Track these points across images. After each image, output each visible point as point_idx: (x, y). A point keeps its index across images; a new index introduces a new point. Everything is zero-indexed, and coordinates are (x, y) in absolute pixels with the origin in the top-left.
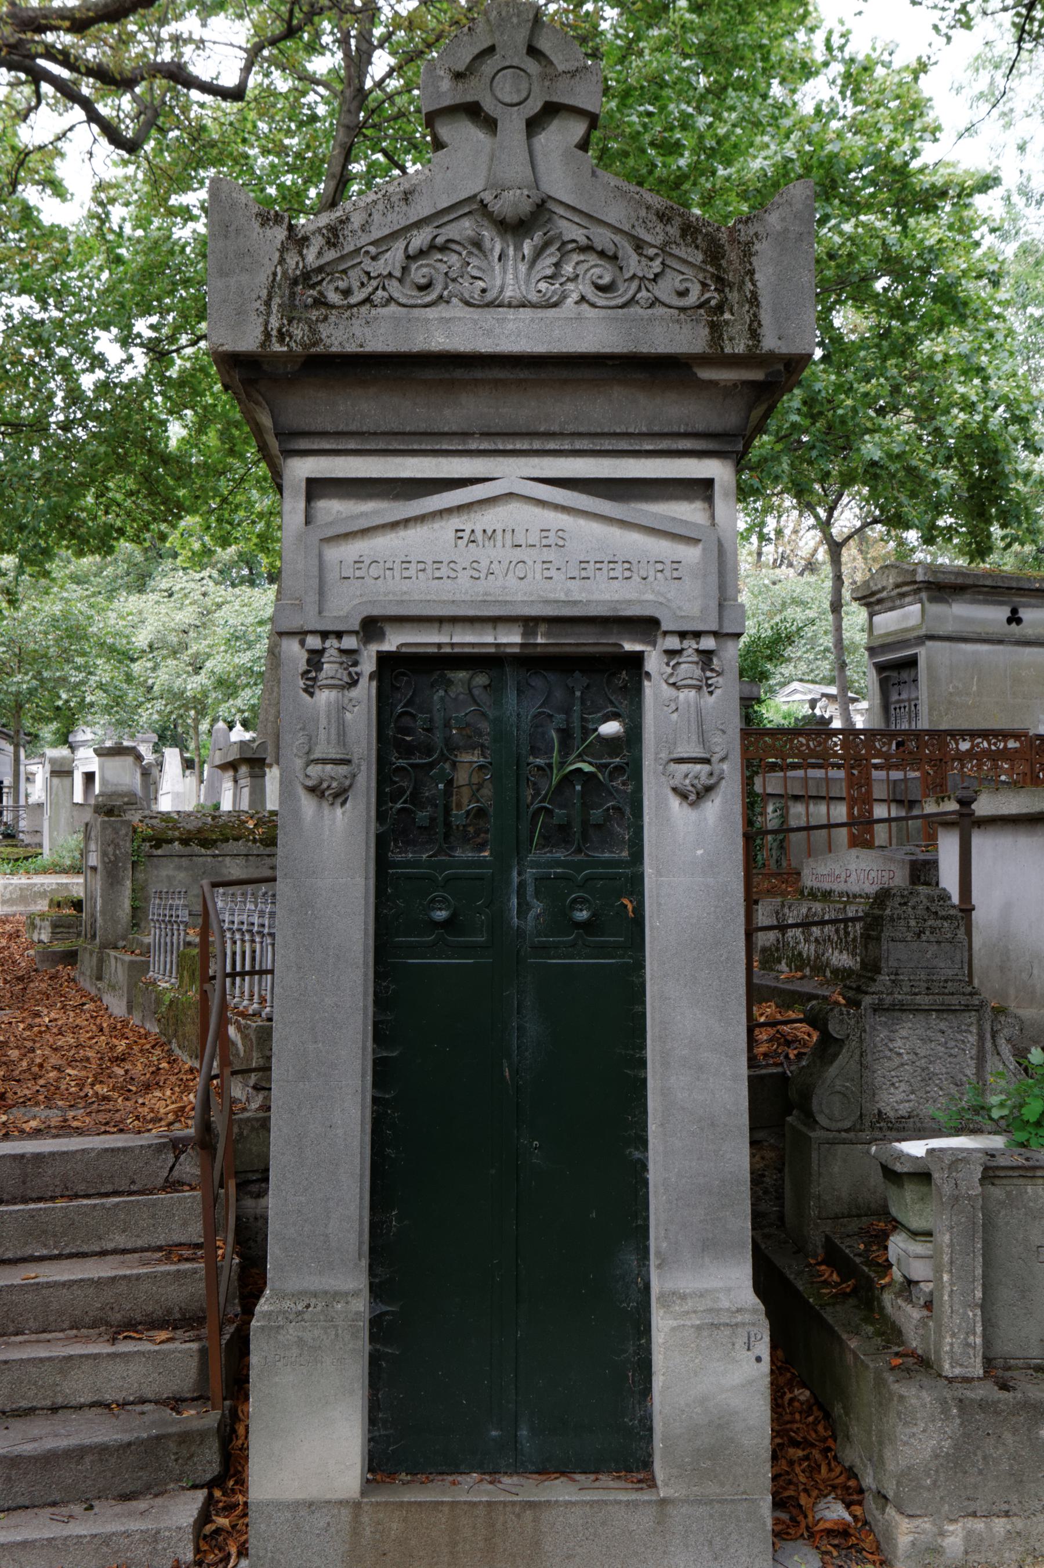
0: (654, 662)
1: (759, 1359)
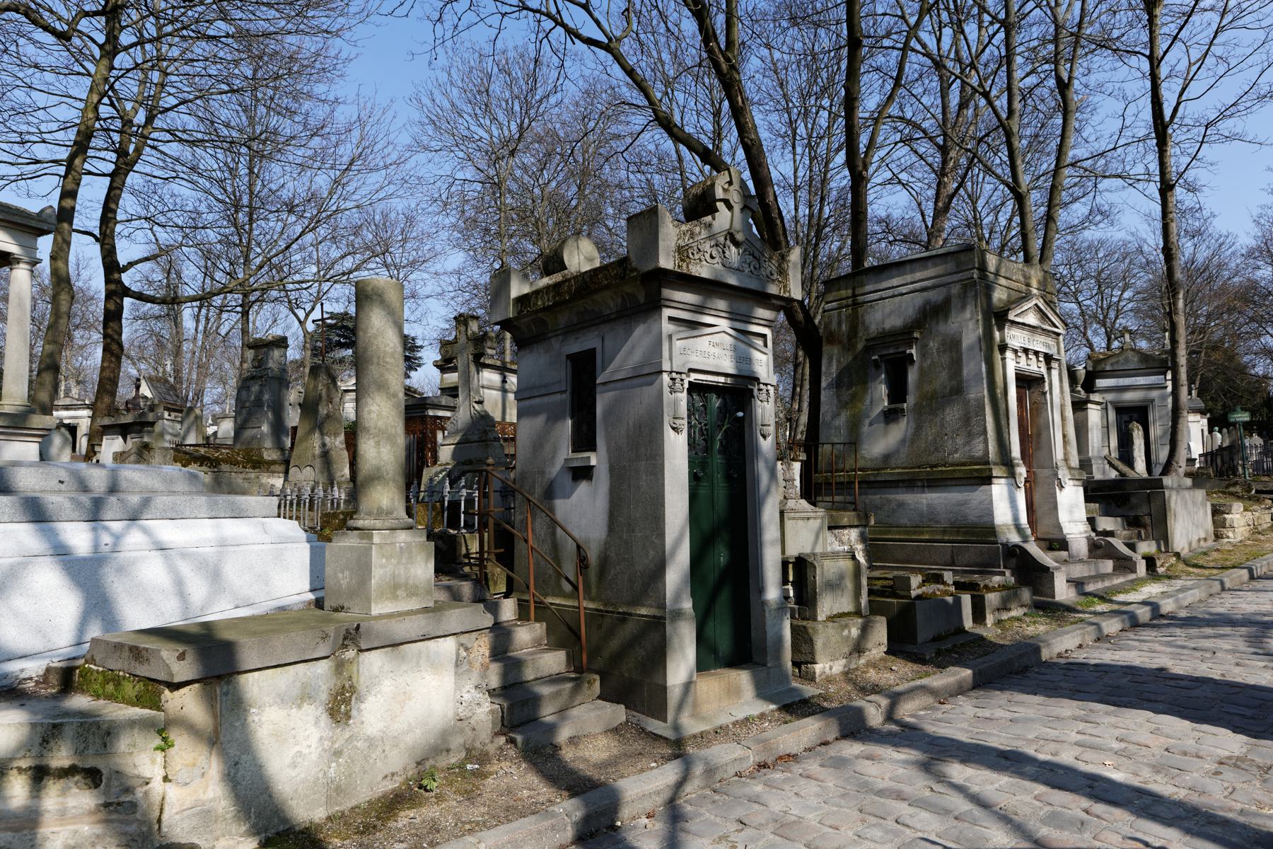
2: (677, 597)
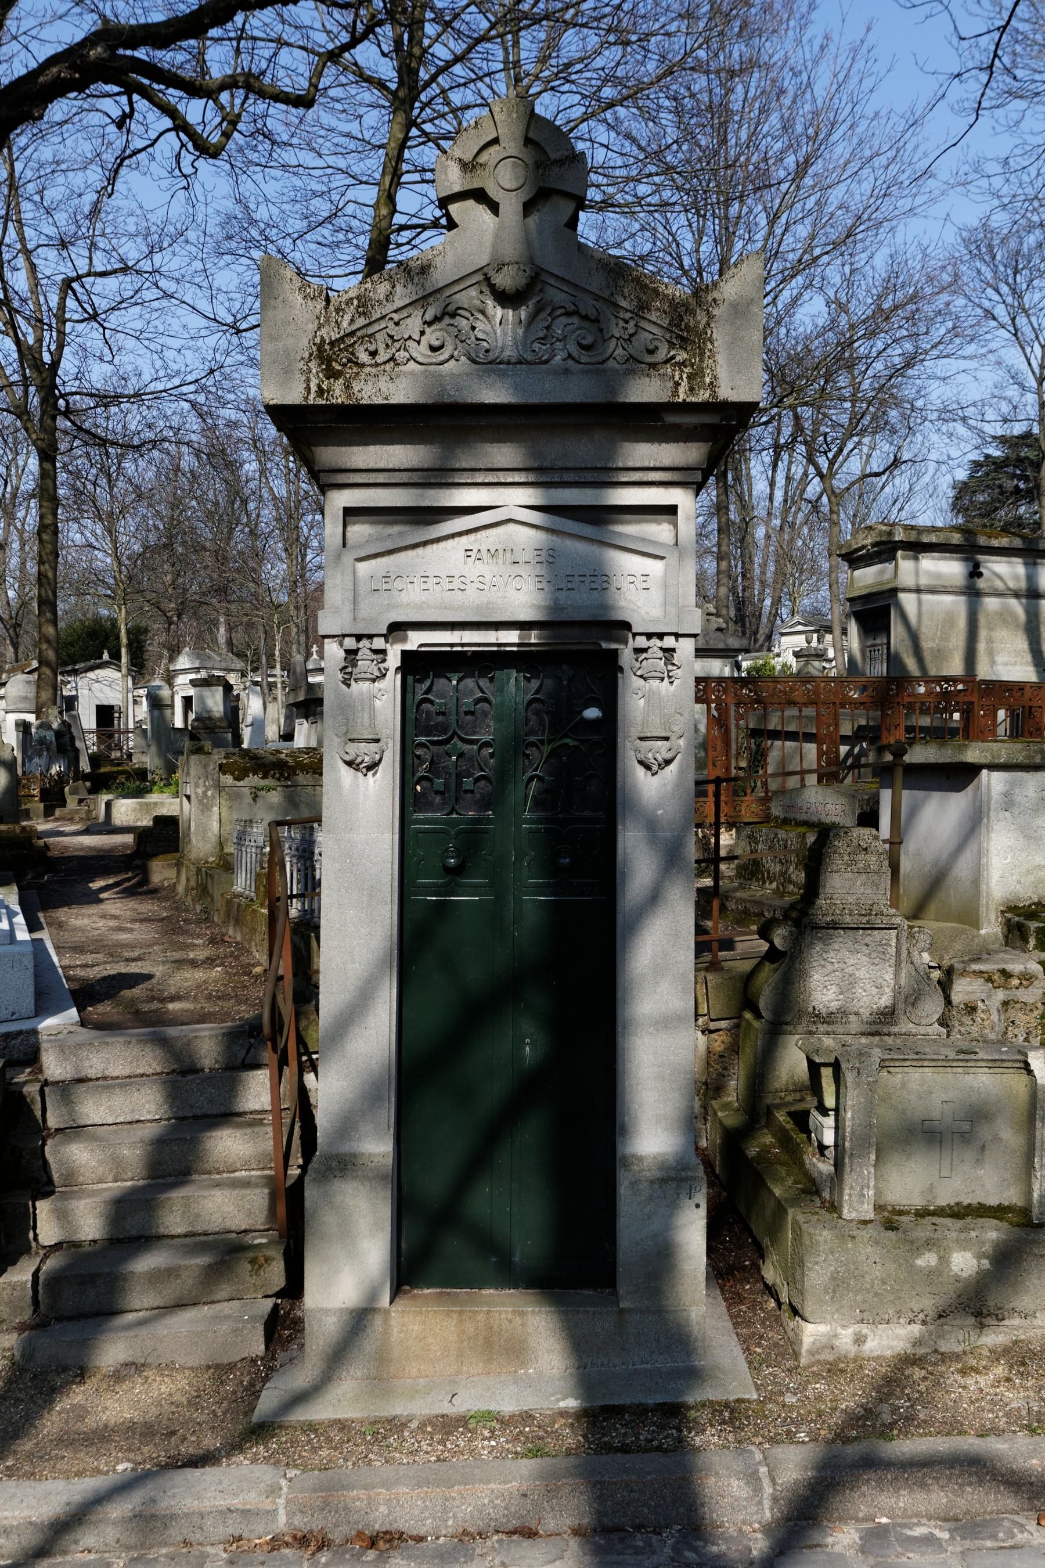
2: (346, 1126)
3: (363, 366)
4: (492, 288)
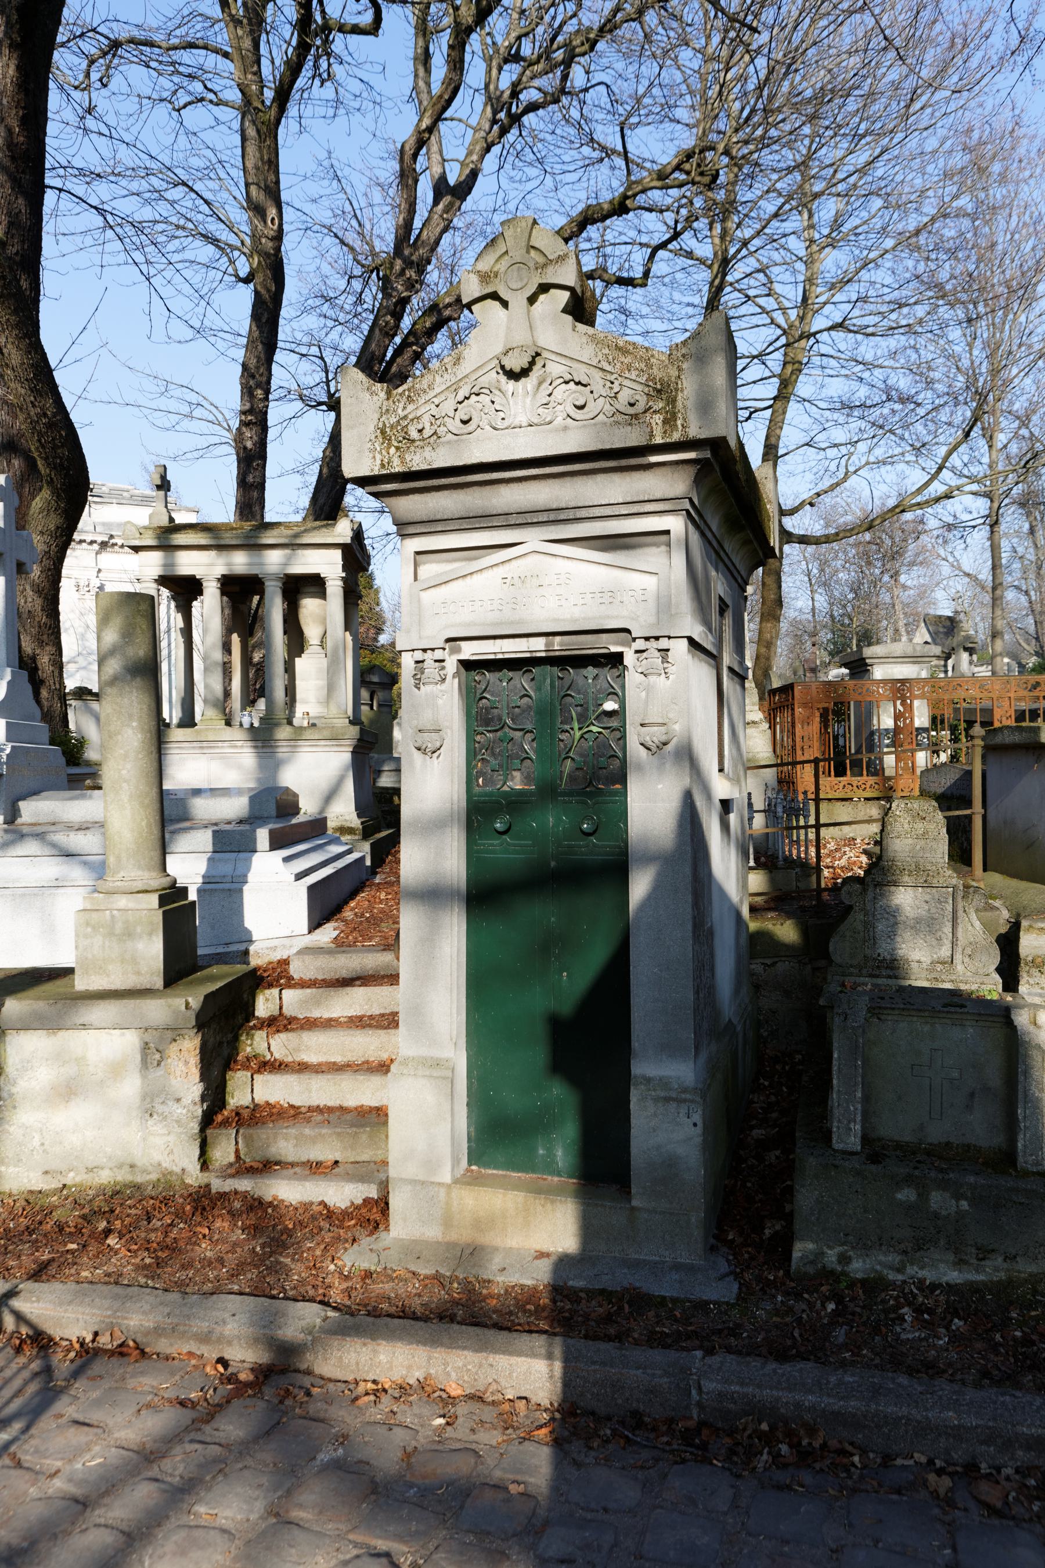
0: (629, 659)
1: (695, 1125)
3: (413, 441)
4: (503, 367)
